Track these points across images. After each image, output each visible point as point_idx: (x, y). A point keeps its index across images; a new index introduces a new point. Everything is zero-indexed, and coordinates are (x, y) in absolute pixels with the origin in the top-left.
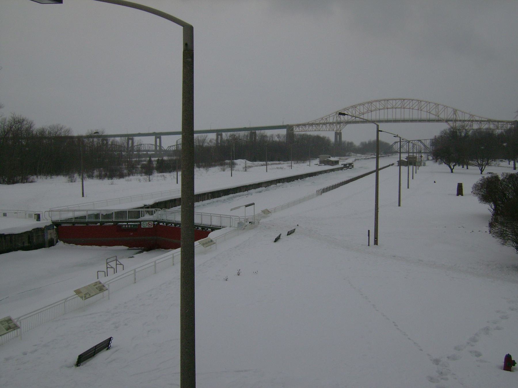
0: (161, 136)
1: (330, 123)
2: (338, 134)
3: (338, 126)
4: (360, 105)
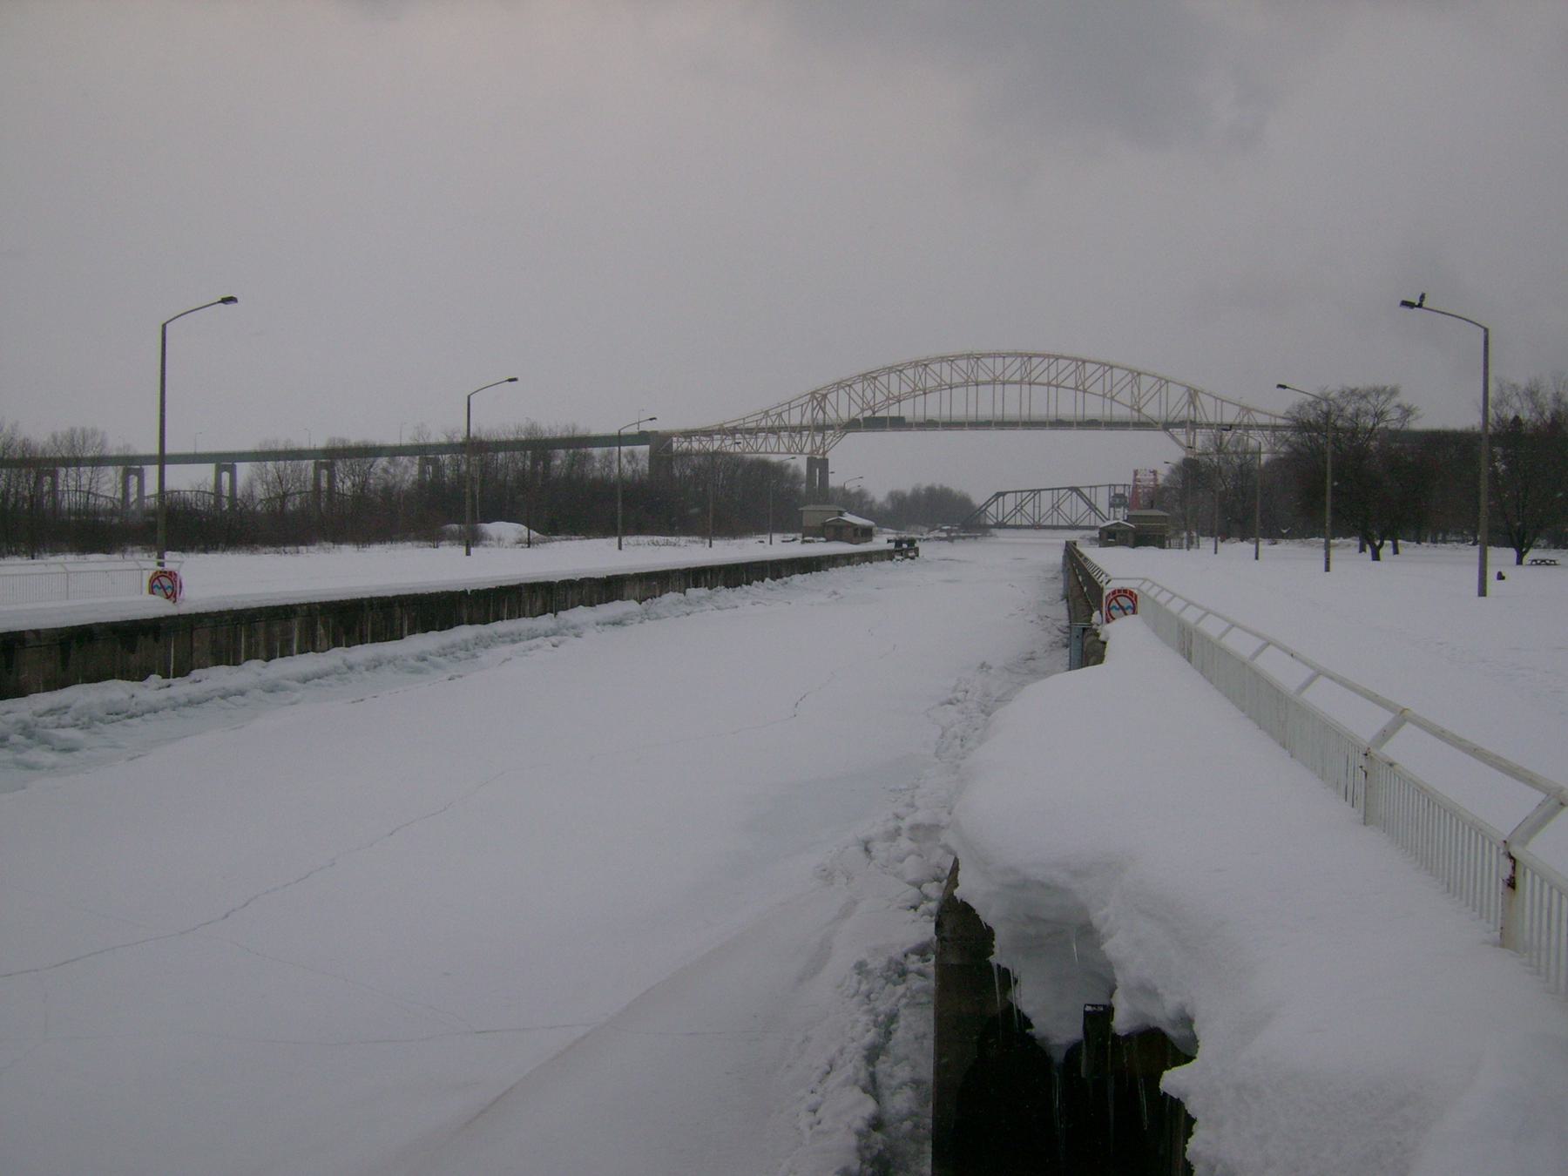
0: (236, 464)
1: (793, 429)
2: (819, 465)
3: (818, 439)
4: (890, 370)
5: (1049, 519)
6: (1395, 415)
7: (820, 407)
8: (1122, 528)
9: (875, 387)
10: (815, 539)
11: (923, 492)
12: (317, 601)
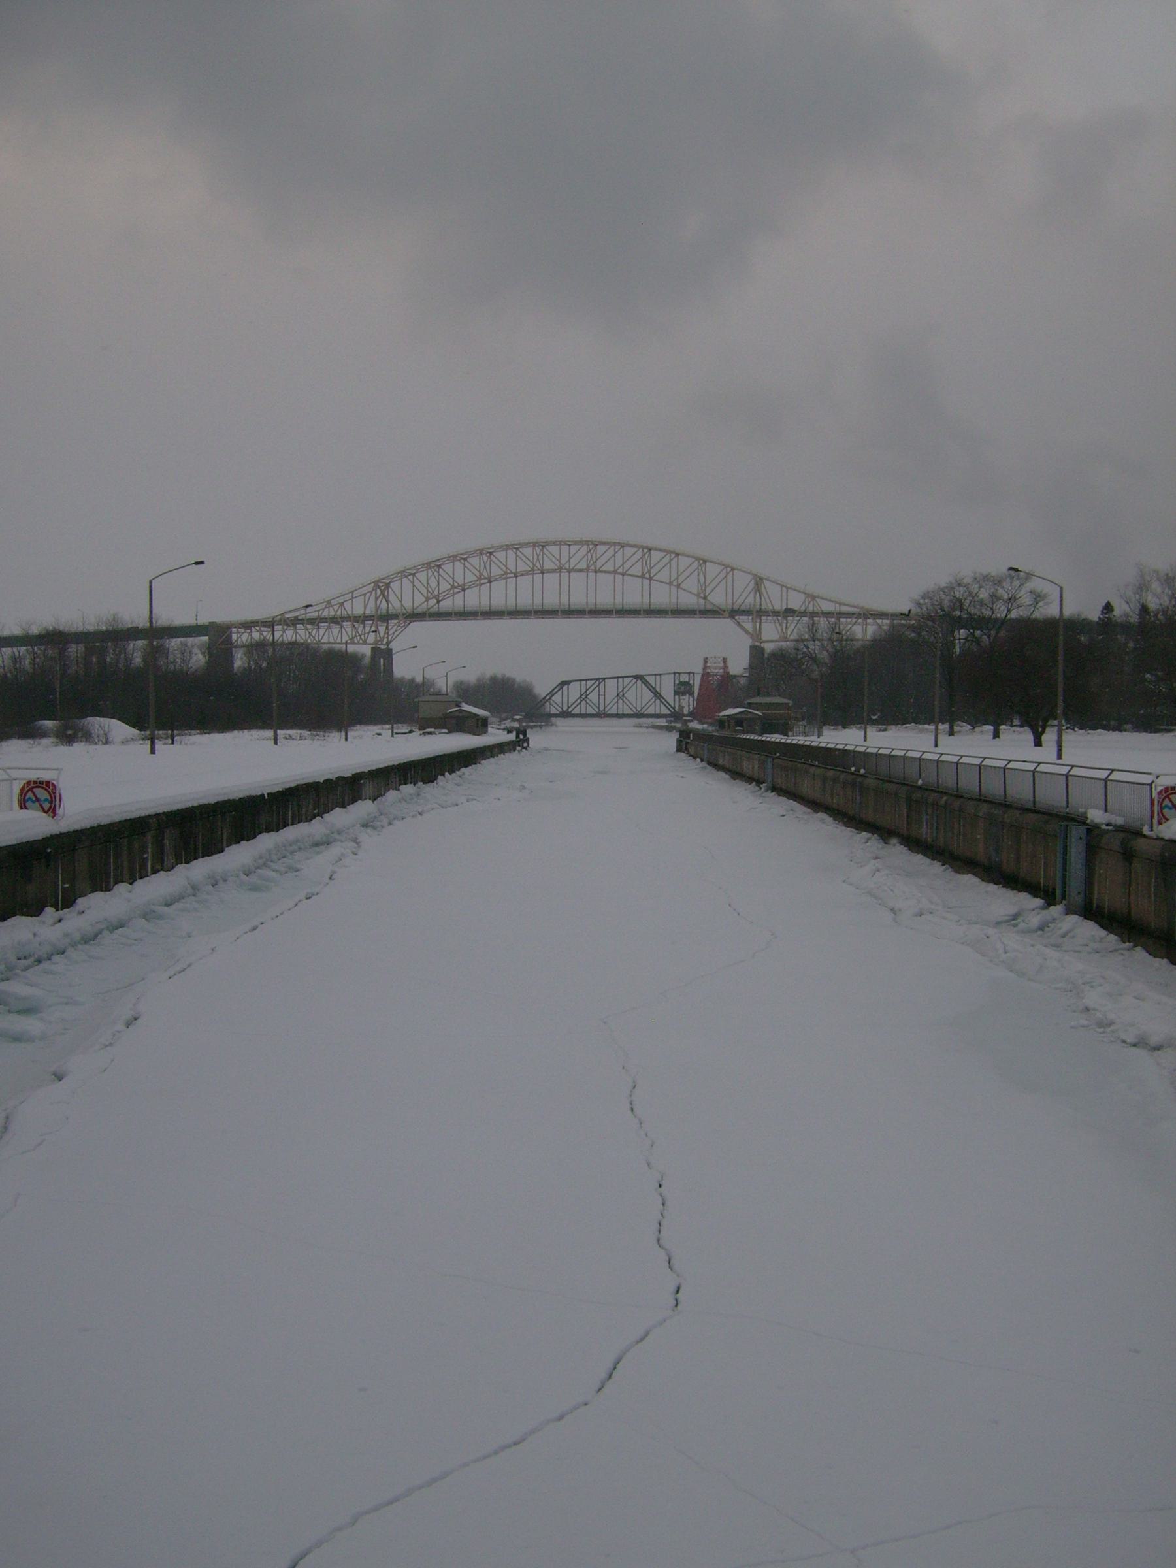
2: (383, 654)
4: (454, 558)
5: (615, 707)
6: (1027, 600)
7: (384, 596)
8: (749, 716)
9: (439, 575)
10: (437, 731)
11: (488, 682)
12: (161, 812)
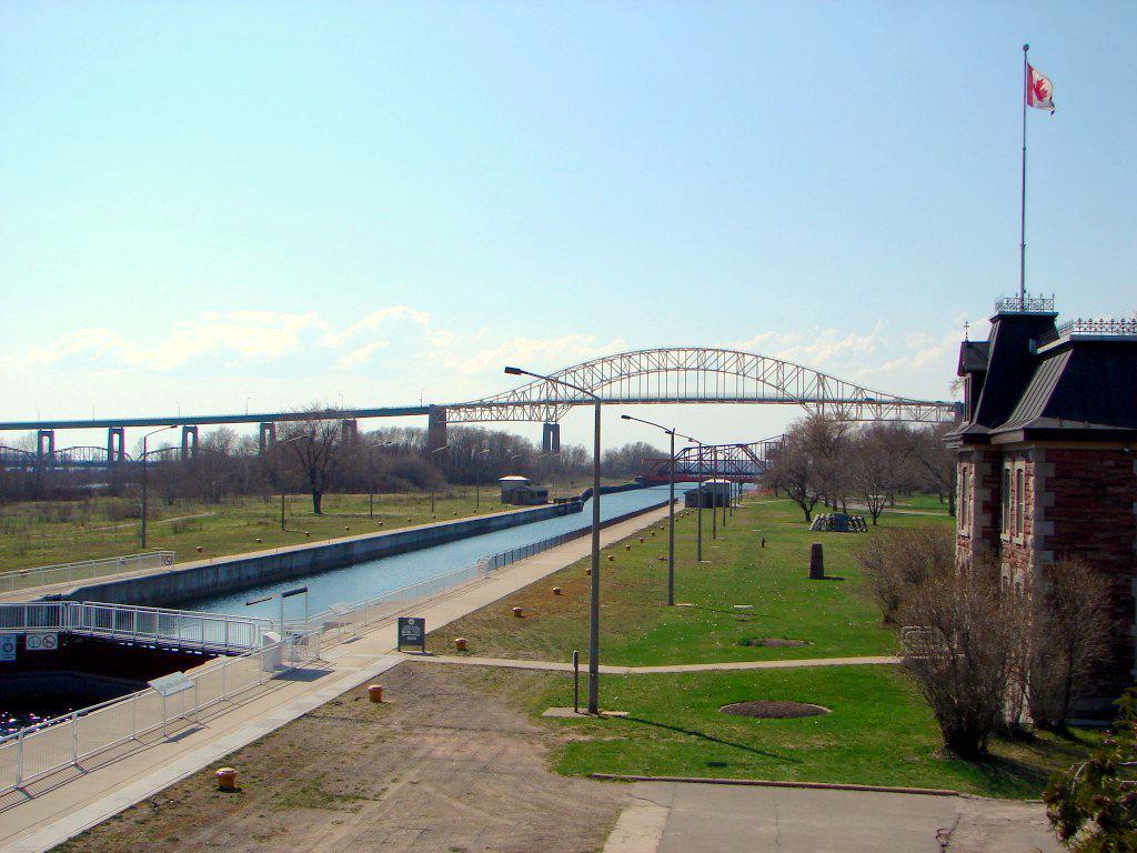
1: (532, 404)
